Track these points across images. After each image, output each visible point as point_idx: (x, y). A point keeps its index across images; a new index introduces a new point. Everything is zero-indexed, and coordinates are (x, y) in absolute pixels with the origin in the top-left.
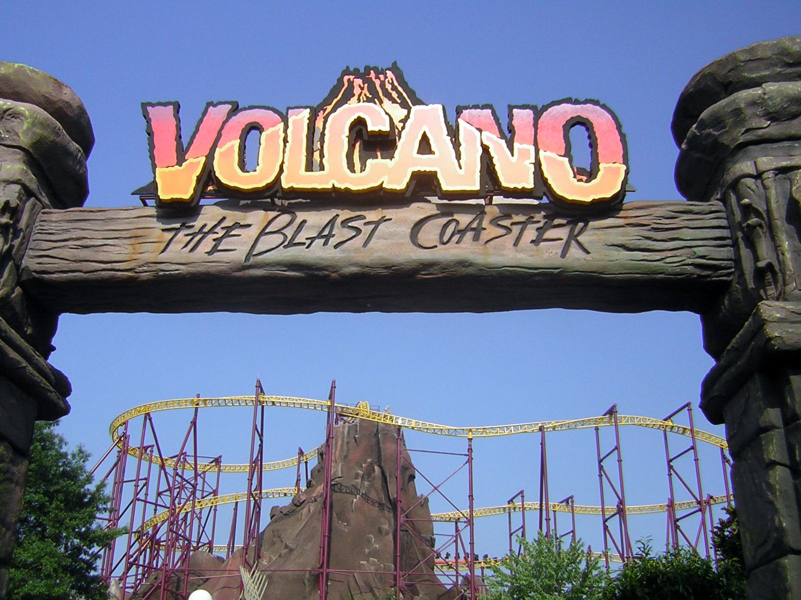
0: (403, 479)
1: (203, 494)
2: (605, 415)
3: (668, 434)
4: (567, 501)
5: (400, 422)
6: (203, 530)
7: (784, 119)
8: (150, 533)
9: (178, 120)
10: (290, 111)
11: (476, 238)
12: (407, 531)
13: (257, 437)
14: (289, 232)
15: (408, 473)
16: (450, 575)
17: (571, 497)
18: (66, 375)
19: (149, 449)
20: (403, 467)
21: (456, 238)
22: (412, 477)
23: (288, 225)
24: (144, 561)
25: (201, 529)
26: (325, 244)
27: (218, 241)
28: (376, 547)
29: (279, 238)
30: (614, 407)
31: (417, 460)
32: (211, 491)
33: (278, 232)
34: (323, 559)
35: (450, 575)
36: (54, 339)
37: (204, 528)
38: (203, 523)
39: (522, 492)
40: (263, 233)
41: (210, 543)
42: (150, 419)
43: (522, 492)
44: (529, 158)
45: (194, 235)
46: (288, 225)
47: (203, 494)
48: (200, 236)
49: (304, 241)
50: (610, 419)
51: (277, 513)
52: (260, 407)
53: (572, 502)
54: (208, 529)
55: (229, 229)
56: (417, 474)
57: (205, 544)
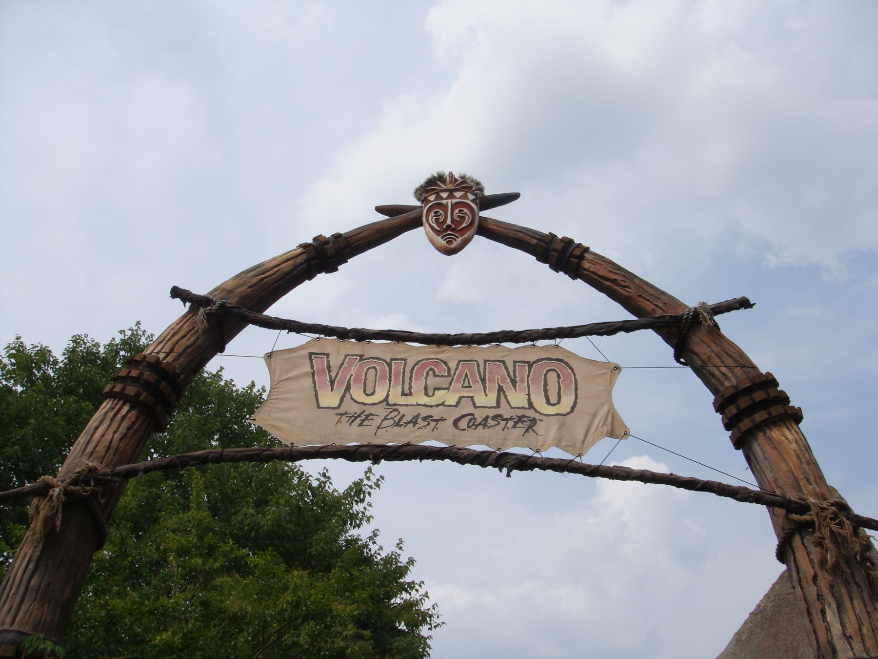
7: (807, 456)
9: (423, 405)
10: (477, 405)
11: (414, 426)
14: (397, 419)
18: (709, 493)
21: (474, 427)
23: (396, 416)
26: (414, 426)
27: (363, 421)
29: (391, 422)
33: (392, 418)
34: (166, 337)
36: (538, 469)
40: (385, 419)
44: (526, 392)
45: (351, 417)
46: (396, 416)
48: (353, 418)
49: (403, 424)
55: (367, 416)
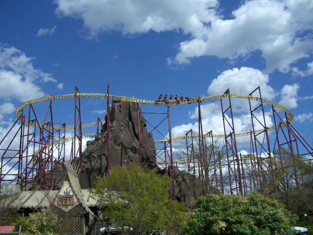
0: (141, 126)
1: (59, 139)
2: (225, 93)
3: (250, 100)
4: (210, 133)
5: (138, 101)
6: (60, 154)
8: (38, 156)
12: (144, 147)
13: (77, 112)
15: (143, 124)
16: (15, 156)
17: (211, 131)
19: (35, 121)
20: (141, 121)
22: (145, 125)
24: (37, 167)
25: (60, 154)
28: (131, 155)
30: (228, 90)
31: (145, 117)
32: (62, 137)
35: (15, 156)
37: (61, 153)
38: (60, 151)
39: (259, 87)
41: (64, 158)
42: (32, 107)
43: (259, 87)
47: (59, 139)
50: (227, 95)
51: (89, 143)
52: (78, 99)
53: (212, 133)
54: (62, 153)
56: (147, 124)
57: (62, 159)
